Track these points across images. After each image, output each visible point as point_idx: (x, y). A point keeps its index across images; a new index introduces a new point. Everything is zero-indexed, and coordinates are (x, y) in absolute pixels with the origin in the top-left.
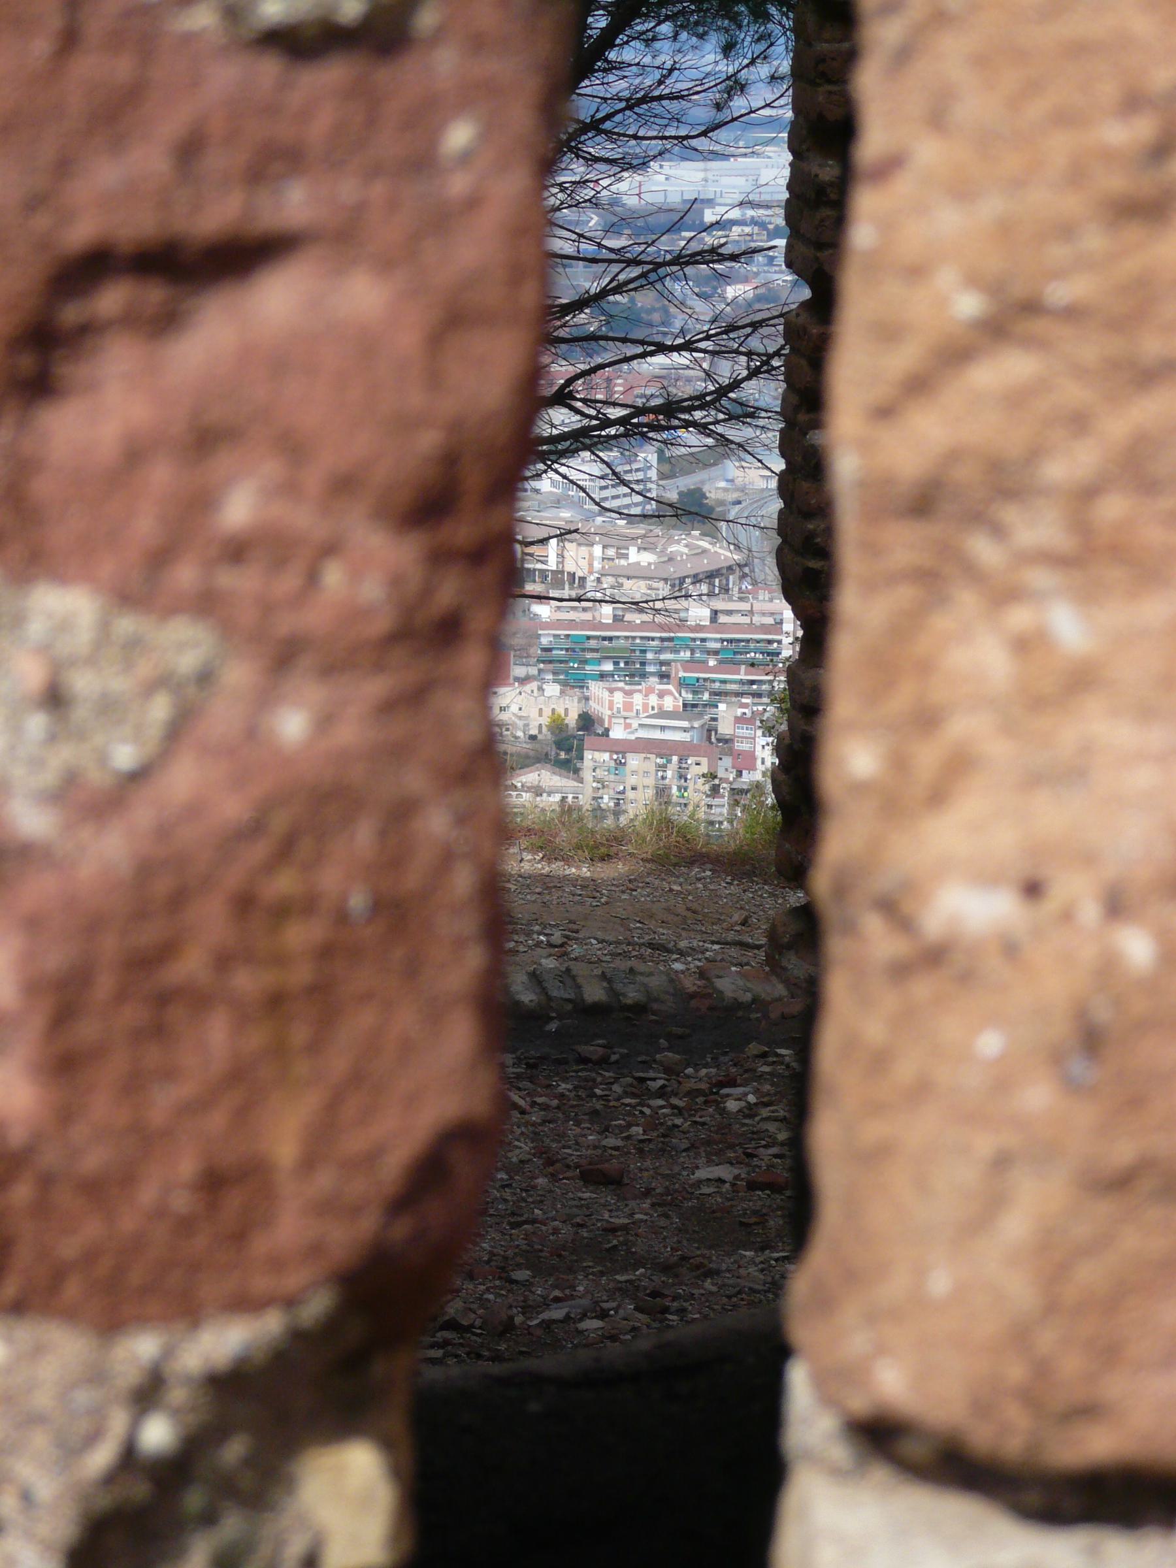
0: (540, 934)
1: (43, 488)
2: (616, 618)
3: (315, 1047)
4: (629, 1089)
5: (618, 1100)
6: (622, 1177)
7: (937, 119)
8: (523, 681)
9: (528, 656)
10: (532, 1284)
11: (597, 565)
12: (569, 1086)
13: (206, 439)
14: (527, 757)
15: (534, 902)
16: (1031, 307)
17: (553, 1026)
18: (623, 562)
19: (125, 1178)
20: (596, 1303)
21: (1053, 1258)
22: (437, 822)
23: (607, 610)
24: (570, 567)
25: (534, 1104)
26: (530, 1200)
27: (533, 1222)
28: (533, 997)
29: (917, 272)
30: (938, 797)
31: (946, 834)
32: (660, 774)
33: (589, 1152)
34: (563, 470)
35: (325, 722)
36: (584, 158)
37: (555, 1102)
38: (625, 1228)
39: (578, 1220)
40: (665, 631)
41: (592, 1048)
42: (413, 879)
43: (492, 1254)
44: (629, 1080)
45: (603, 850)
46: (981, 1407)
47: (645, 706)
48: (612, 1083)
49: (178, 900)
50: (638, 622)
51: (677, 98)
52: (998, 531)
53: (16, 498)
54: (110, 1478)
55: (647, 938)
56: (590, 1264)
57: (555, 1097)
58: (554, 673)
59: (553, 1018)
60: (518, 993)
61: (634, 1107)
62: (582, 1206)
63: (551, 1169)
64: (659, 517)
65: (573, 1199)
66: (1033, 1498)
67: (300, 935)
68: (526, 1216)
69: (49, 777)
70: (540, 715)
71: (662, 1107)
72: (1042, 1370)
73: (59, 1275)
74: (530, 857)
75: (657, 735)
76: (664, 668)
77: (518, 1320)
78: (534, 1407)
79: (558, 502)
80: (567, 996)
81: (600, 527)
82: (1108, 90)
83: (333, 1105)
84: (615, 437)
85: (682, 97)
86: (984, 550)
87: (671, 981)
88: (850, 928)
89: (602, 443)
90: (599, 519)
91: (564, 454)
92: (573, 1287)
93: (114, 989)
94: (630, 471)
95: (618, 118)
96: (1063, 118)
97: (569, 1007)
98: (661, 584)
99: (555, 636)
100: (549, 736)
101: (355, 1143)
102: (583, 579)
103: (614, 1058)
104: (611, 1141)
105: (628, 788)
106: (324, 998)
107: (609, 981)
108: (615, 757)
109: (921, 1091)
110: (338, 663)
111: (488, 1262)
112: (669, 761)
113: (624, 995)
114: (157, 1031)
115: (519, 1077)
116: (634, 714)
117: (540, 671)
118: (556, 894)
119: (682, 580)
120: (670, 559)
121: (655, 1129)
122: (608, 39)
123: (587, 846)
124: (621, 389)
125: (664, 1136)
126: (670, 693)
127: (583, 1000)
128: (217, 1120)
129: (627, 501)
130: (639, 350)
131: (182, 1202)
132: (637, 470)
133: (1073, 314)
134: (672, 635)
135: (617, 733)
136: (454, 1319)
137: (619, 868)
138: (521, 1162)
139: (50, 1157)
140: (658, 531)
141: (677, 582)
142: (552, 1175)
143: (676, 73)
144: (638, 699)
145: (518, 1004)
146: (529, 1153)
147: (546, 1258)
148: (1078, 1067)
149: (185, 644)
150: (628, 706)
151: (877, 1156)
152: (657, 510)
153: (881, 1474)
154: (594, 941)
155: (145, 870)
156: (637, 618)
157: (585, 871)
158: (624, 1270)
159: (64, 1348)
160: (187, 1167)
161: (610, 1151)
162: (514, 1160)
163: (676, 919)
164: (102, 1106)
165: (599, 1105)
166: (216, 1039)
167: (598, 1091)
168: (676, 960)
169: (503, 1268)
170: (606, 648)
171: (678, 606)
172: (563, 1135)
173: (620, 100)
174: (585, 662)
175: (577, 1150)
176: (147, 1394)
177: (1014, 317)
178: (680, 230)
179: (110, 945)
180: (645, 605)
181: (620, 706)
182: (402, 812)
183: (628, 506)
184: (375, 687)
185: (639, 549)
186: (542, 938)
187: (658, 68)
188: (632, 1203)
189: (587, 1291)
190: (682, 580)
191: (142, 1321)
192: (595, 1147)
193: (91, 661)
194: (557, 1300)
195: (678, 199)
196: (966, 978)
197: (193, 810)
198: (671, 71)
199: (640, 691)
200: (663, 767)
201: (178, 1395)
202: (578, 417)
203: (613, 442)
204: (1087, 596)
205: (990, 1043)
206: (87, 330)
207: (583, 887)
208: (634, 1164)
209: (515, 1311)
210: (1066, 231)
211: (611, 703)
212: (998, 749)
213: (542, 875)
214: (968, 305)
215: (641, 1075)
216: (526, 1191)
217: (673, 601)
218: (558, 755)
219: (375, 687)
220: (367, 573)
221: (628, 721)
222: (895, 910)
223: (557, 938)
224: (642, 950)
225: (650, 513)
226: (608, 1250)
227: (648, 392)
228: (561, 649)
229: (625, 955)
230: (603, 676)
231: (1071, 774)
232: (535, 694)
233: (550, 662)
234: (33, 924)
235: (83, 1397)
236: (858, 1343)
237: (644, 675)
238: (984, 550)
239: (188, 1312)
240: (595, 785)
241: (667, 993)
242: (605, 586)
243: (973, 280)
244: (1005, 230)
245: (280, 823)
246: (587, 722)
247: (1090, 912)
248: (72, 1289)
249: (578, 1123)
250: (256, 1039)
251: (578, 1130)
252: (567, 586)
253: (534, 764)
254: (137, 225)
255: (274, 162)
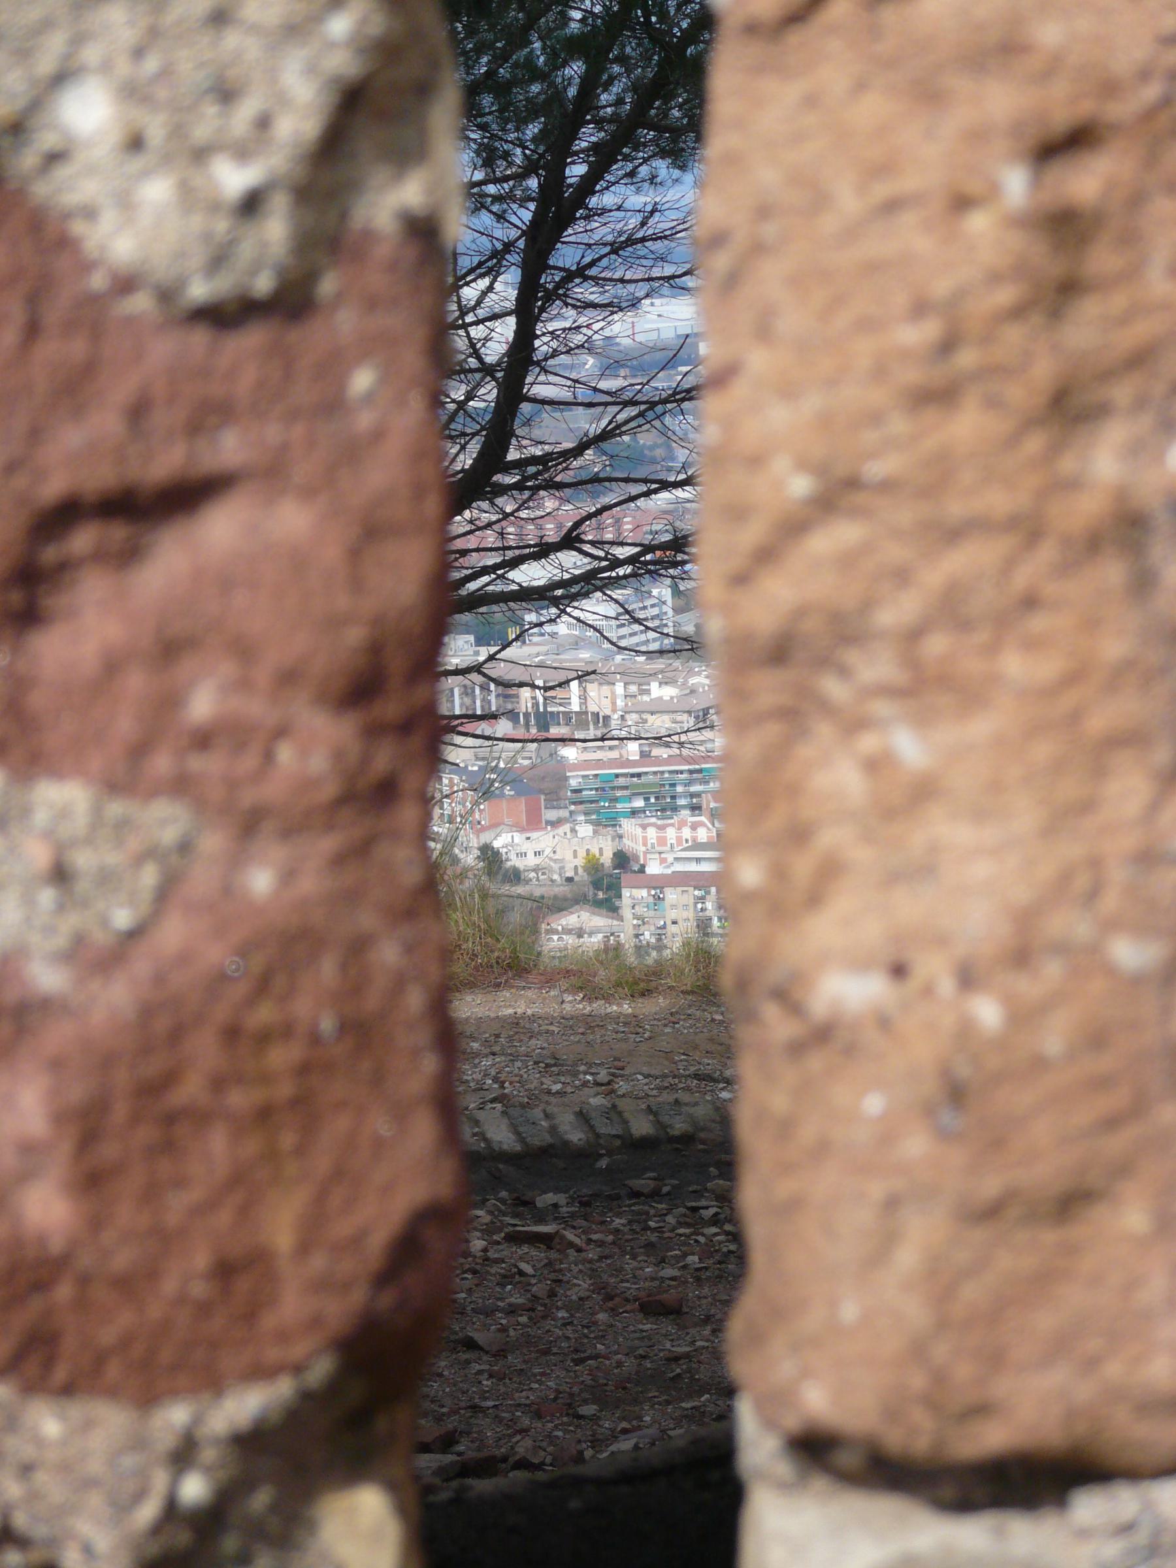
0: (586, 1073)
1: (37, 700)
2: (644, 755)
3: (300, 1151)
4: (681, 1220)
5: (672, 1230)
6: (681, 1306)
7: (764, 332)
8: (556, 824)
9: (559, 799)
10: (599, 1418)
11: (620, 703)
12: (623, 1221)
13: (170, 649)
14: (565, 899)
15: (579, 1042)
16: (853, 483)
17: (603, 1163)
18: (646, 698)
19: (151, 1274)
20: (664, 1431)
21: (940, 1283)
22: (388, 954)
23: (633, 748)
24: (592, 708)
25: (590, 1241)
26: (592, 1335)
27: (596, 1357)
28: (582, 1136)
29: (756, 461)
30: (814, 899)
31: (823, 930)
32: (699, 906)
33: (647, 1284)
34: (576, 613)
35: (288, 876)
36: (574, 306)
37: (611, 1238)
38: (687, 1356)
39: (641, 1351)
40: (690, 764)
41: (643, 1182)
42: (372, 1001)
43: (558, 1392)
44: (682, 1210)
45: (642, 985)
46: (892, 1413)
47: (679, 839)
48: (666, 1215)
49: (176, 1035)
50: (665, 756)
51: (660, 238)
52: (844, 672)
53: (16, 710)
54: (157, 1529)
55: (692, 1069)
56: (657, 1394)
57: (611, 1233)
58: (586, 814)
59: (602, 1155)
60: (566, 1133)
61: (688, 1236)
62: (643, 1338)
63: (610, 1304)
64: (675, 651)
65: (635, 1332)
66: (948, 1492)
67: (282, 1057)
68: (589, 1352)
69: (60, 941)
70: (575, 856)
71: (716, 1234)
72: (940, 1378)
73: (100, 1360)
74: (570, 998)
75: (693, 867)
76: (694, 800)
77: (588, 1453)
78: (574, 1504)
79: (577, 644)
80: (614, 1132)
81: (619, 665)
82: (900, 299)
83: (321, 1197)
84: (625, 577)
85: (665, 237)
86: (834, 688)
87: (717, 1109)
88: (752, 1017)
89: (612, 584)
90: (619, 658)
91: (574, 597)
92: (640, 1418)
93: (128, 1115)
94: (645, 608)
95: (604, 262)
96: (867, 325)
97: (618, 1143)
98: (685, 717)
99: (584, 777)
100: (586, 877)
101: (342, 1228)
102: (607, 718)
103: (665, 1189)
104: (669, 1272)
105: (669, 923)
106: (305, 1108)
107: (656, 1114)
108: (653, 892)
109: (822, 1150)
110: (294, 827)
111: (556, 1399)
112: (708, 893)
113: (671, 1126)
114: (168, 1147)
115: (573, 1215)
116: (668, 848)
117: (571, 813)
118: (599, 1033)
119: (706, 712)
120: (693, 692)
121: (711, 1256)
122: (588, 186)
123: (627, 982)
124: (629, 527)
125: (720, 1263)
126: (702, 824)
127: (631, 1135)
128: (224, 1218)
129: (643, 637)
130: (643, 488)
131: (199, 1289)
132: (653, 606)
133: (887, 486)
134: (697, 767)
135: (653, 868)
136: (524, 1458)
137: (659, 1004)
138: (581, 1299)
139: (85, 1260)
140: (677, 664)
141: (701, 714)
142: (613, 1310)
143: (657, 214)
144: (671, 833)
145: (566, 1143)
146: (588, 1290)
147: (612, 1391)
148: (947, 1118)
149: (165, 820)
150: (662, 841)
151: (793, 1206)
152: (676, 644)
153: (820, 1483)
154: (640, 1077)
155: (147, 1012)
156: (664, 753)
157: (627, 1008)
158: (690, 1396)
159: (110, 1420)
160: (201, 1260)
161: (668, 1282)
162: (574, 1297)
163: (719, 1048)
164: (127, 1214)
165: (653, 1237)
166: (217, 1149)
167: (652, 1224)
168: (722, 1089)
169: (570, 1405)
170: (636, 785)
171: (702, 738)
172: (620, 1270)
173: (605, 245)
174: (615, 800)
175: (635, 1283)
176: (183, 1456)
177: (838, 493)
178: (674, 367)
179: (122, 1078)
180: (668, 739)
181: (654, 841)
182: (358, 947)
183: (637, 645)
184: (328, 844)
185: (660, 684)
186: (588, 1077)
187: (639, 211)
188: (693, 1331)
189: (654, 1421)
190: (706, 712)
191: (174, 1393)
192: (653, 1279)
193: (89, 840)
194: (625, 1431)
195: (672, 335)
196: (850, 1051)
197: (184, 958)
198: (652, 212)
199: (672, 825)
200: (702, 899)
201: (209, 1454)
202: (587, 560)
203: (624, 582)
204: (922, 721)
205: (874, 1104)
206: (64, 567)
207: (626, 1024)
208: (692, 1293)
209: (584, 1446)
210: (875, 418)
211: (645, 839)
212: (861, 855)
213: (584, 1015)
214: (800, 486)
215: (694, 1204)
216: (588, 1327)
217: (698, 733)
218: (596, 895)
219: (328, 844)
220: (314, 749)
221: (663, 856)
222: (787, 997)
223: (603, 1076)
224: (689, 1082)
225: (669, 647)
226: (672, 1379)
227: (655, 527)
228: (591, 789)
229: (672, 1088)
230: (634, 813)
231: (924, 870)
232: (569, 836)
233: (581, 803)
234: (57, 1065)
235: (129, 1461)
236: (786, 1368)
237: (675, 809)
238: (834, 688)
239: (212, 1383)
240: (635, 922)
241: (713, 1121)
242: (630, 723)
243: (803, 465)
244: (825, 422)
245: (258, 962)
246: (622, 860)
247: (946, 986)
248: (113, 1371)
249: (634, 1258)
250: (251, 1146)
251: (635, 1264)
252: (591, 727)
253: (572, 906)
254: (99, 478)
255: (209, 415)
